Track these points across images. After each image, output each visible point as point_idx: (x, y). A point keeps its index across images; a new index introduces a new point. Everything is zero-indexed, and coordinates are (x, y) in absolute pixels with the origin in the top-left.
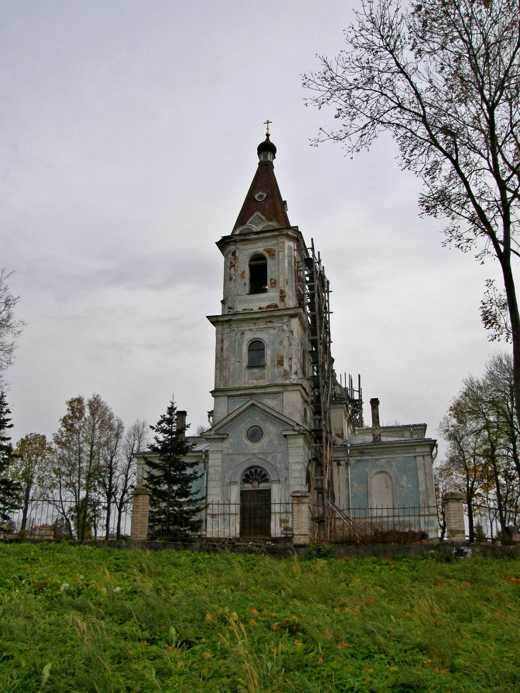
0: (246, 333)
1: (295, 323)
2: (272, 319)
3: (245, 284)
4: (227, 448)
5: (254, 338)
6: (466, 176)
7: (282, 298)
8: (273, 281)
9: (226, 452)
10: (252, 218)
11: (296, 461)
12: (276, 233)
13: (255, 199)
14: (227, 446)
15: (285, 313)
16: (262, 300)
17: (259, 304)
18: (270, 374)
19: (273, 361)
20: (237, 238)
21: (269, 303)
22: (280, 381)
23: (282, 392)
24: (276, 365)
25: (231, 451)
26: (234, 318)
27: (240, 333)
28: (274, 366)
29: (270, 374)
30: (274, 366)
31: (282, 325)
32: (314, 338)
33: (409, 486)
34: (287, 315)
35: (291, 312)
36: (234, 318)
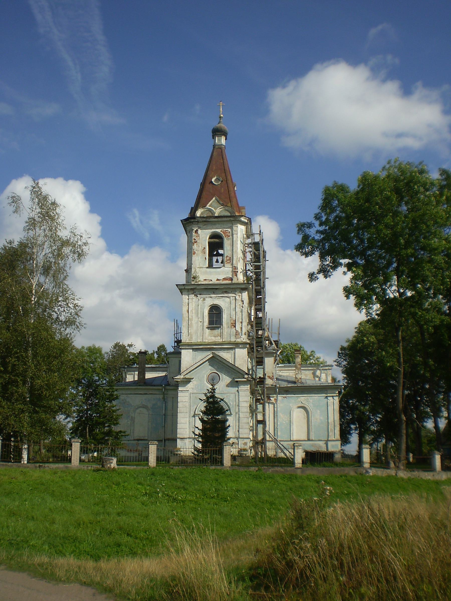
0: (206, 299)
1: (245, 295)
2: (227, 290)
3: (206, 258)
4: (193, 389)
5: (213, 304)
6: (225, 379)
7: (235, 272)
8: (228, 258)
9: (192, 392)
10: (211, 202)
11: (245, 400)
12: (232, 219)
13: (212, 182)
14: (192, 387)
15: (239, 286)
16: (219, 273)
17: (217, 276)
18: (226, 333)
19: (227, 323)
20: (200, 220)
21: (225, 277)
22: (233, 339)
23: (235, 348)
24: (230, 326)
25: (195, 391)
26: (198, 287)
27: (202, 299)
28: (228, 327)
29: (226, 333)
30: (228, 327)
31: (235, 295)
32: (257, 287)
33: (321, 418)
34: (239, 288)
35: (243, 286)
36: (198, 287)
